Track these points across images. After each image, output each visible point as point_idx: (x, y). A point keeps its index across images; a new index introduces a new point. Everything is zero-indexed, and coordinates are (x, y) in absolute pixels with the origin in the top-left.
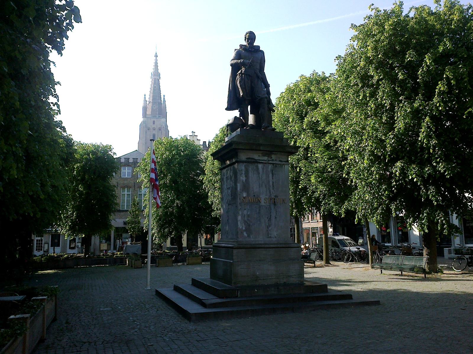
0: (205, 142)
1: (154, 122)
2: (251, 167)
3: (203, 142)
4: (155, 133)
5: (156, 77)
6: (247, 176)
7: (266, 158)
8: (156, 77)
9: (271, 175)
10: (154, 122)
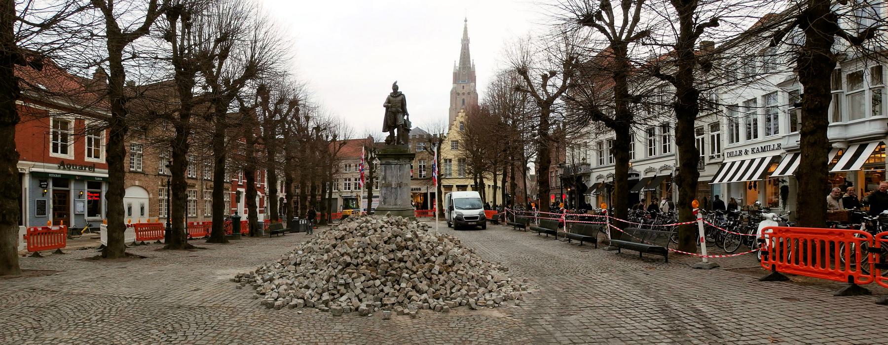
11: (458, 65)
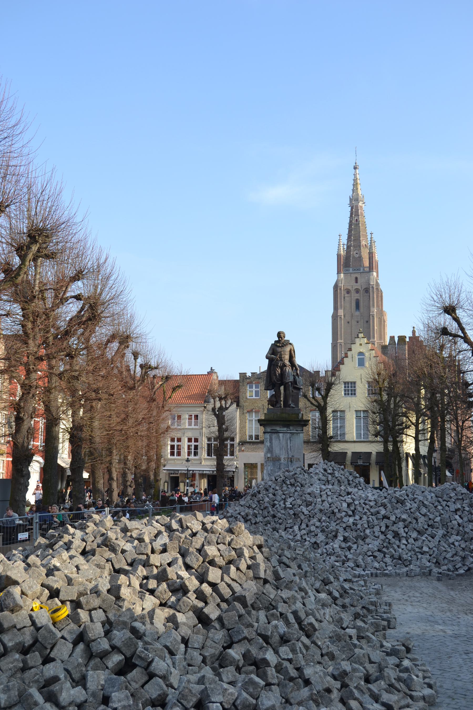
0: (392, 338)
1: (356, 279)
2: (274, 436)
3: (391, 337)
4: (358, 298)
5: (355, 185)
6: (271, 442)
7: (285, 429)
8: (355, 185)
9: (289, 441)
10: (356, 279)
11: (344, 240)
